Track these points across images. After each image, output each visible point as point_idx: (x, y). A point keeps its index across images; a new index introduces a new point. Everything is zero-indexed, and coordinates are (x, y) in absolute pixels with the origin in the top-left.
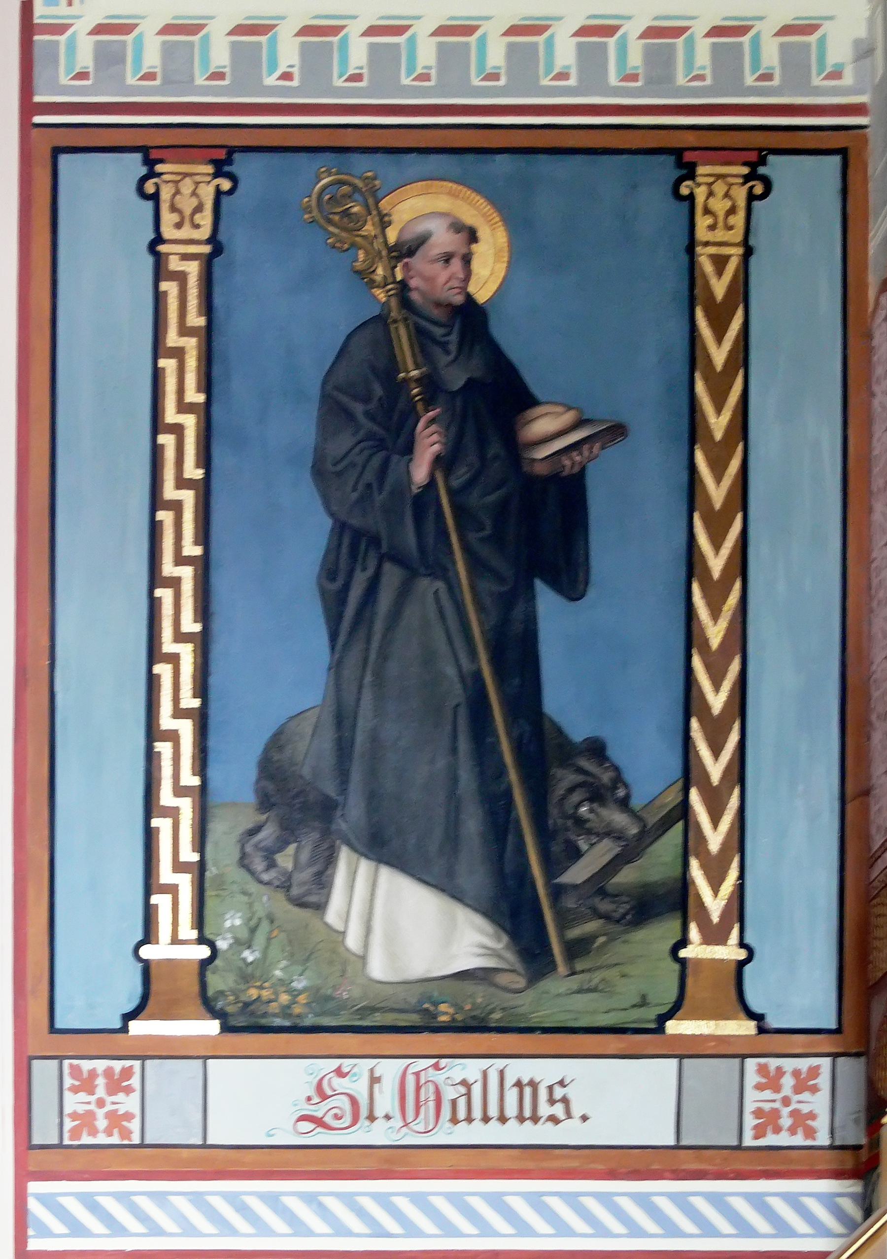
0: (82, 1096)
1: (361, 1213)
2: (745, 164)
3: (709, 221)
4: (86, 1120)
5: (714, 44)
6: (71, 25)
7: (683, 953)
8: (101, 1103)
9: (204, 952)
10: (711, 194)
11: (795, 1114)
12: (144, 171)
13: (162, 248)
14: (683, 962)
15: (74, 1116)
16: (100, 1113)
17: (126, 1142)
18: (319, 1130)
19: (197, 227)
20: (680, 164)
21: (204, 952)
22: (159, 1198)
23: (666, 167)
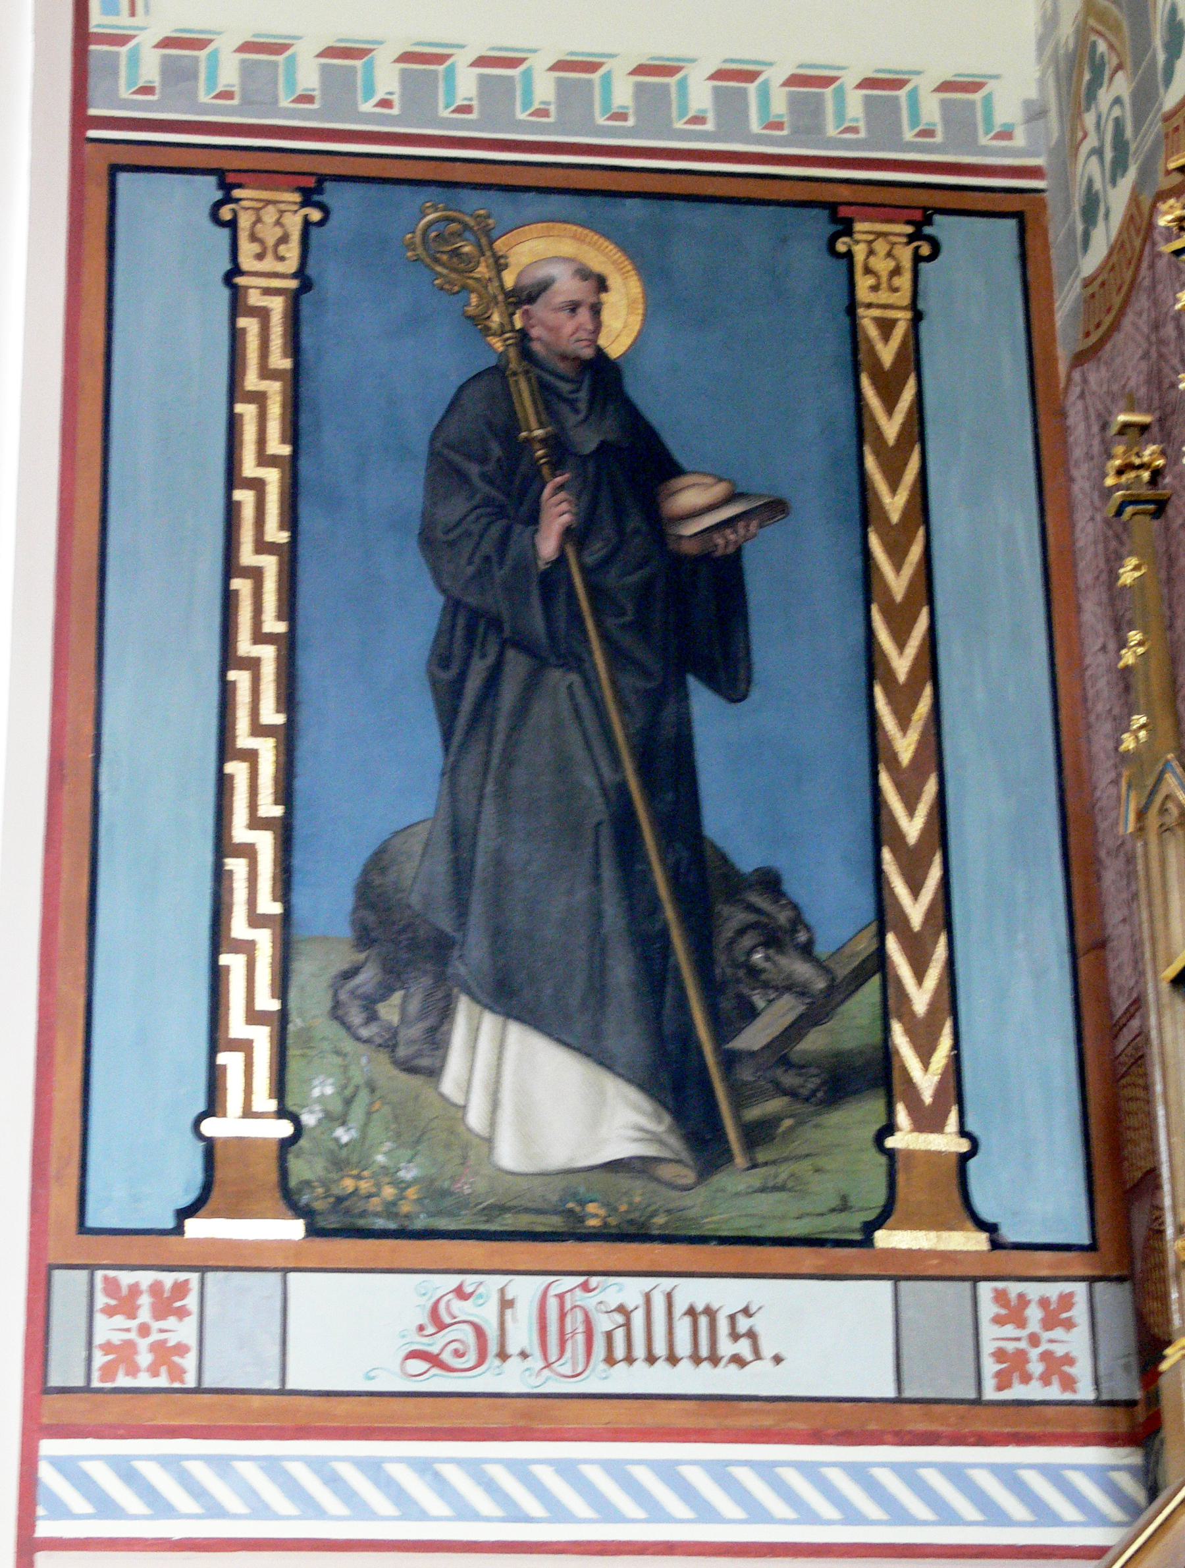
0: (120, 1321)
3: (871, 281)
4: (124, 1354)
7: (890, 1142)
8: (144, 1330)
9: (285, 1129)
10: (871, 252)
11: (1046, 1356)
13: (240, 281)
14: (891, 1154)
15: (108, 1347)
16: (143, 1344)
17: (177, 1385)
18: (435, 1371)
21: (285, 1129)
22: (221, 1464)
23: (818, 224)
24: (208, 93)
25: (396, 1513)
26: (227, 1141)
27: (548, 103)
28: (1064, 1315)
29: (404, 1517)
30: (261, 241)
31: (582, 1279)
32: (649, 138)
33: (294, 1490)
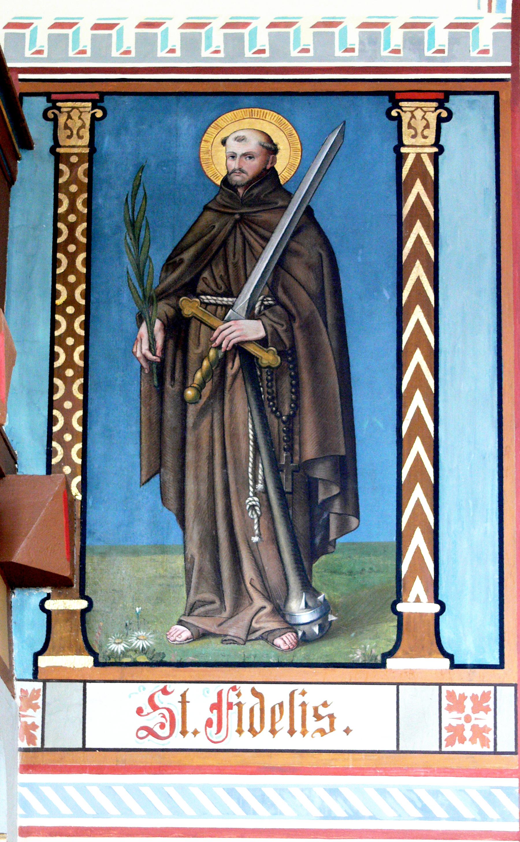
0: (455, 714)
1: (67, 799)
6: (297, 22)
7: (400, 607)
10: (69, 117)
11: (474, 728)
12: (390, 105)
13: (403, 150)
14: (49, 613)
15: (450, 728)
16: (468, 727)
17: (32, 746)
18: (150, 737)
19: (425, 137)
20: (48, 101)
24: (118, 50)
25: (420, 815)
26: (410, 614)
27: (43, 47)
28: (485, 705)
30: (415, 129)
31: (162, 685)
32: (101, 62)
33: (118, 802)
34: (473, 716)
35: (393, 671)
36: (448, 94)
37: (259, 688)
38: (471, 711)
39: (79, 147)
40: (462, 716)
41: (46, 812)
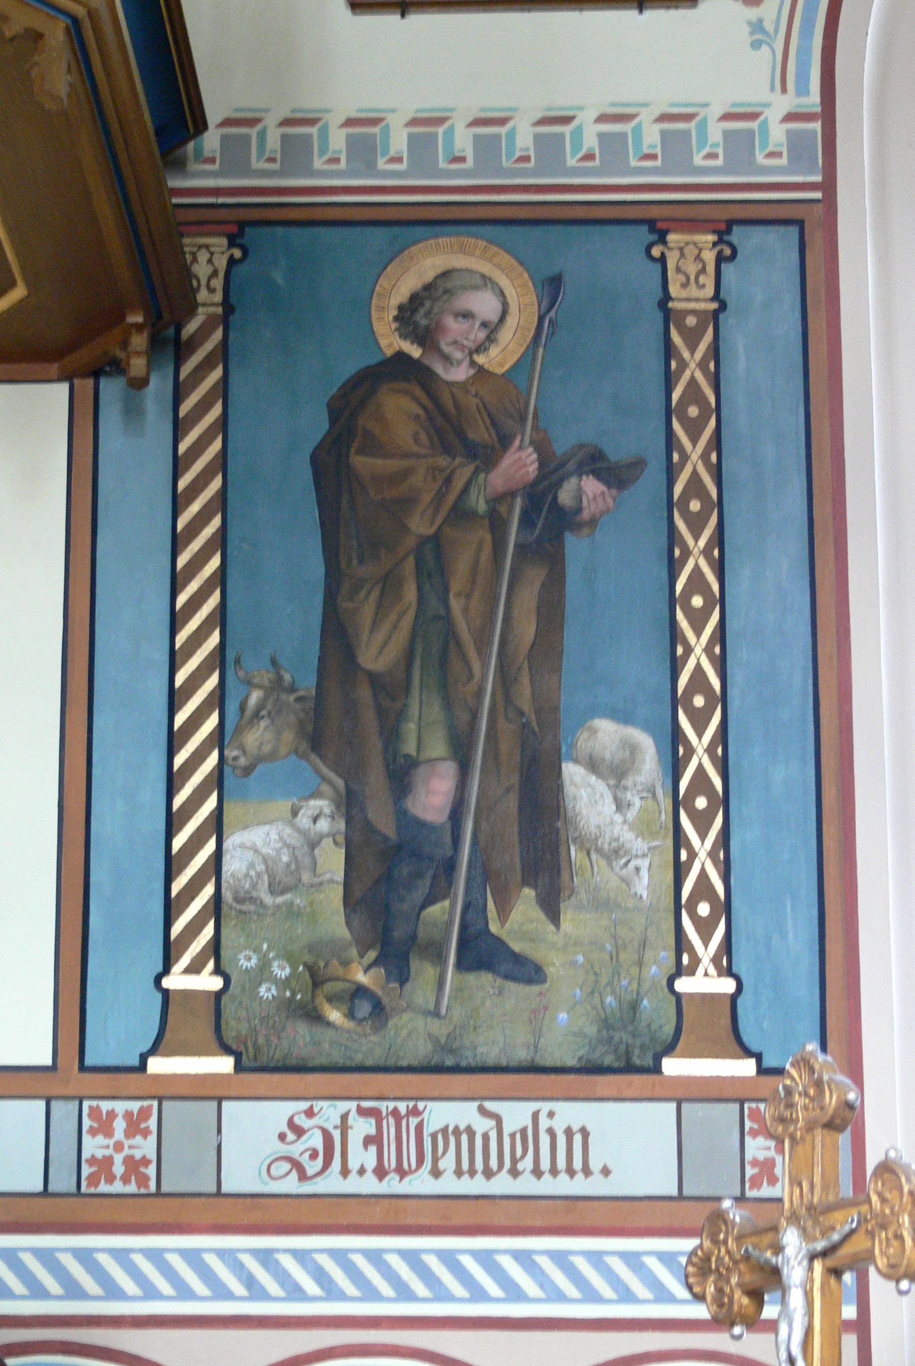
0: (100, 1139)
2: (714, 232)
5: (816, 133)
14: (166, 993)
15: (93, 1161)
16: (118, 1159)
17: (143, 1191)
23: (643, 234)
28: (143, 1126)
29: (548, 1300)
34: (127, 1143)
35: (157, 1077)
36: (730, 224)
37: (490, 1106)
38: (123, 1135)
39: (697, 300)
40: (111, 1142)
41: (540, 1294)
